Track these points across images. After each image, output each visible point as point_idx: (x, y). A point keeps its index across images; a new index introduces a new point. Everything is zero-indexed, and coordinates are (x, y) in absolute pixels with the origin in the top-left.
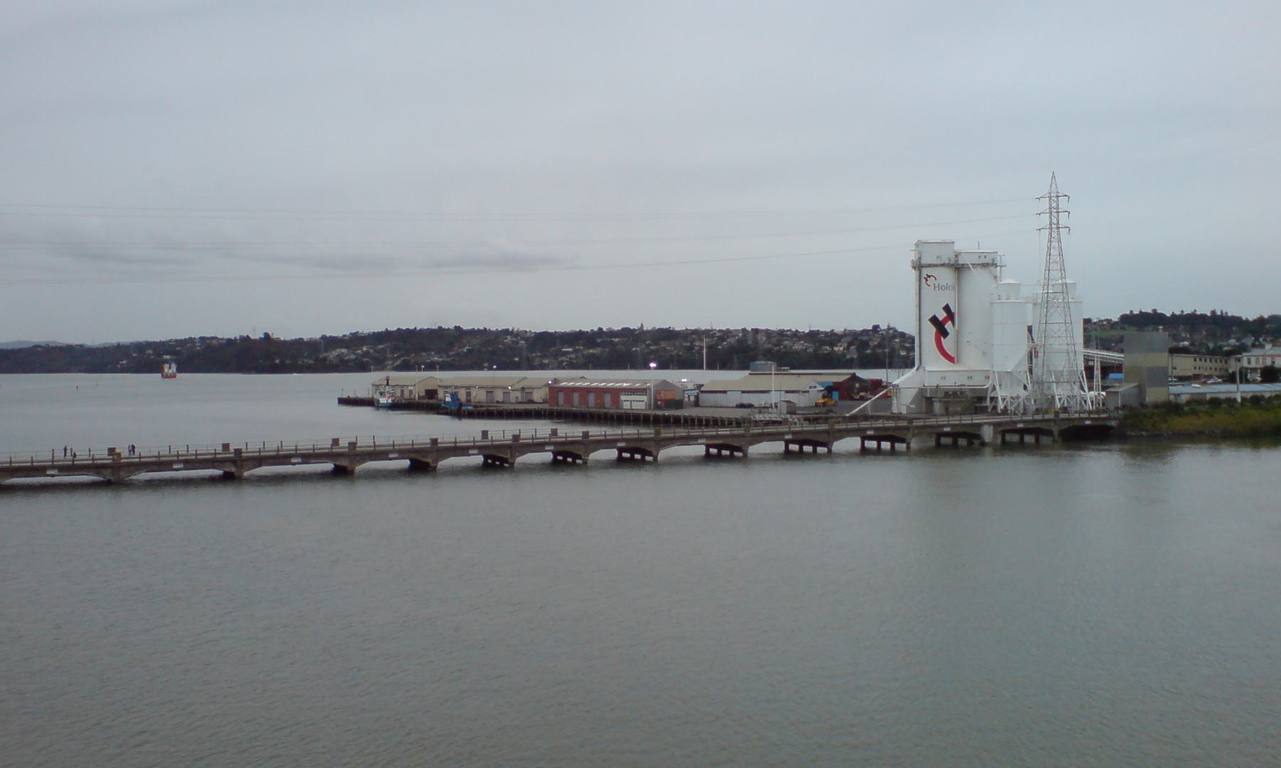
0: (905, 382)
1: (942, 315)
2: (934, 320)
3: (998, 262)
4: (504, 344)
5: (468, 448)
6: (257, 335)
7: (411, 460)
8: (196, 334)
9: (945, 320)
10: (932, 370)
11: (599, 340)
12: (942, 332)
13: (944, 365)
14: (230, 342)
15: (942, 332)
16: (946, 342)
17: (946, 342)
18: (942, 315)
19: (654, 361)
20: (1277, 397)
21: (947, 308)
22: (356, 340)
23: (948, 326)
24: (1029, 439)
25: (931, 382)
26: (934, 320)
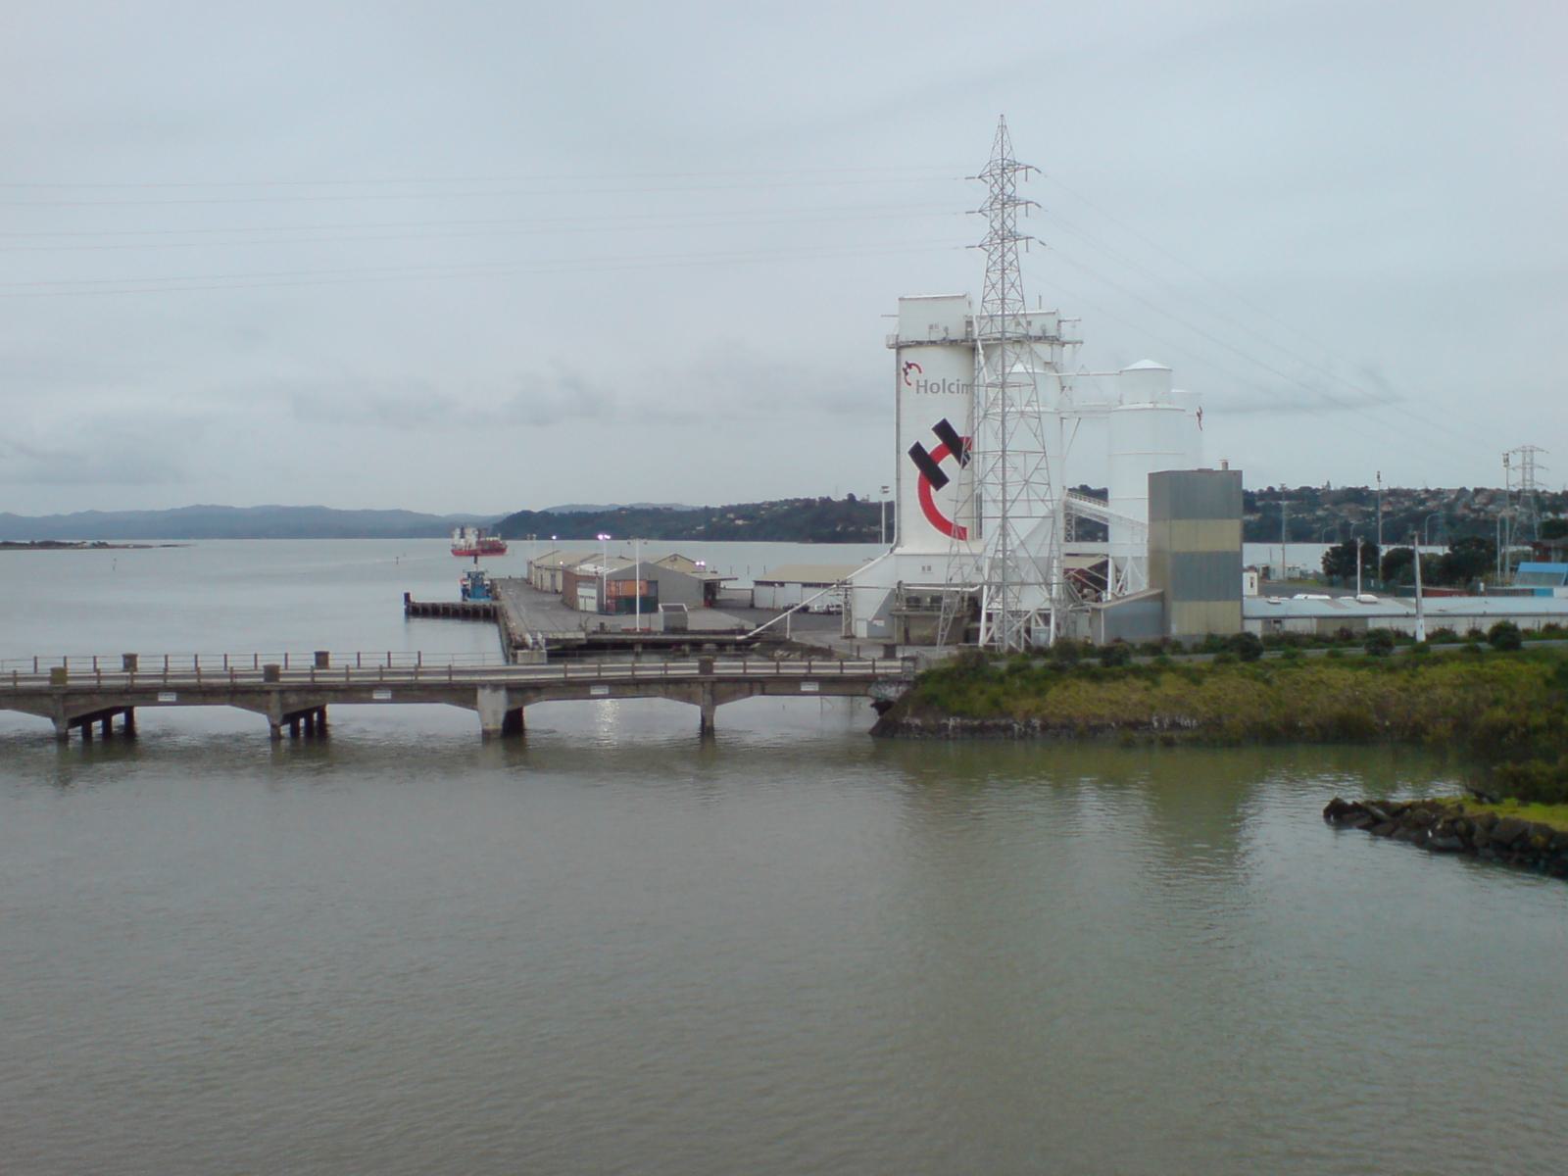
0: (871, 576)
1: (932, 443)
2: (917, 453)
3: (1067, 332)
4: (1534, 551)
5: (372, 687)
6: (840, 496)
7: (278, 681)
8: (750, 502)
9: (940, 453)
10: (918, 556)
11: (1259, 504)
12: (933, 477)
13: (938, 542)
14: (518, 513)
15: (933, 477)
16: (940, 497)
17: (938, 497)
18: (932, 443)
19: (555, 534)
20: (1552, 631)
21: (944, 429)
22: (742, 511)
23: (948, 464)
24: (743, 647)
25: (914, 578)
26: (917, 453)
